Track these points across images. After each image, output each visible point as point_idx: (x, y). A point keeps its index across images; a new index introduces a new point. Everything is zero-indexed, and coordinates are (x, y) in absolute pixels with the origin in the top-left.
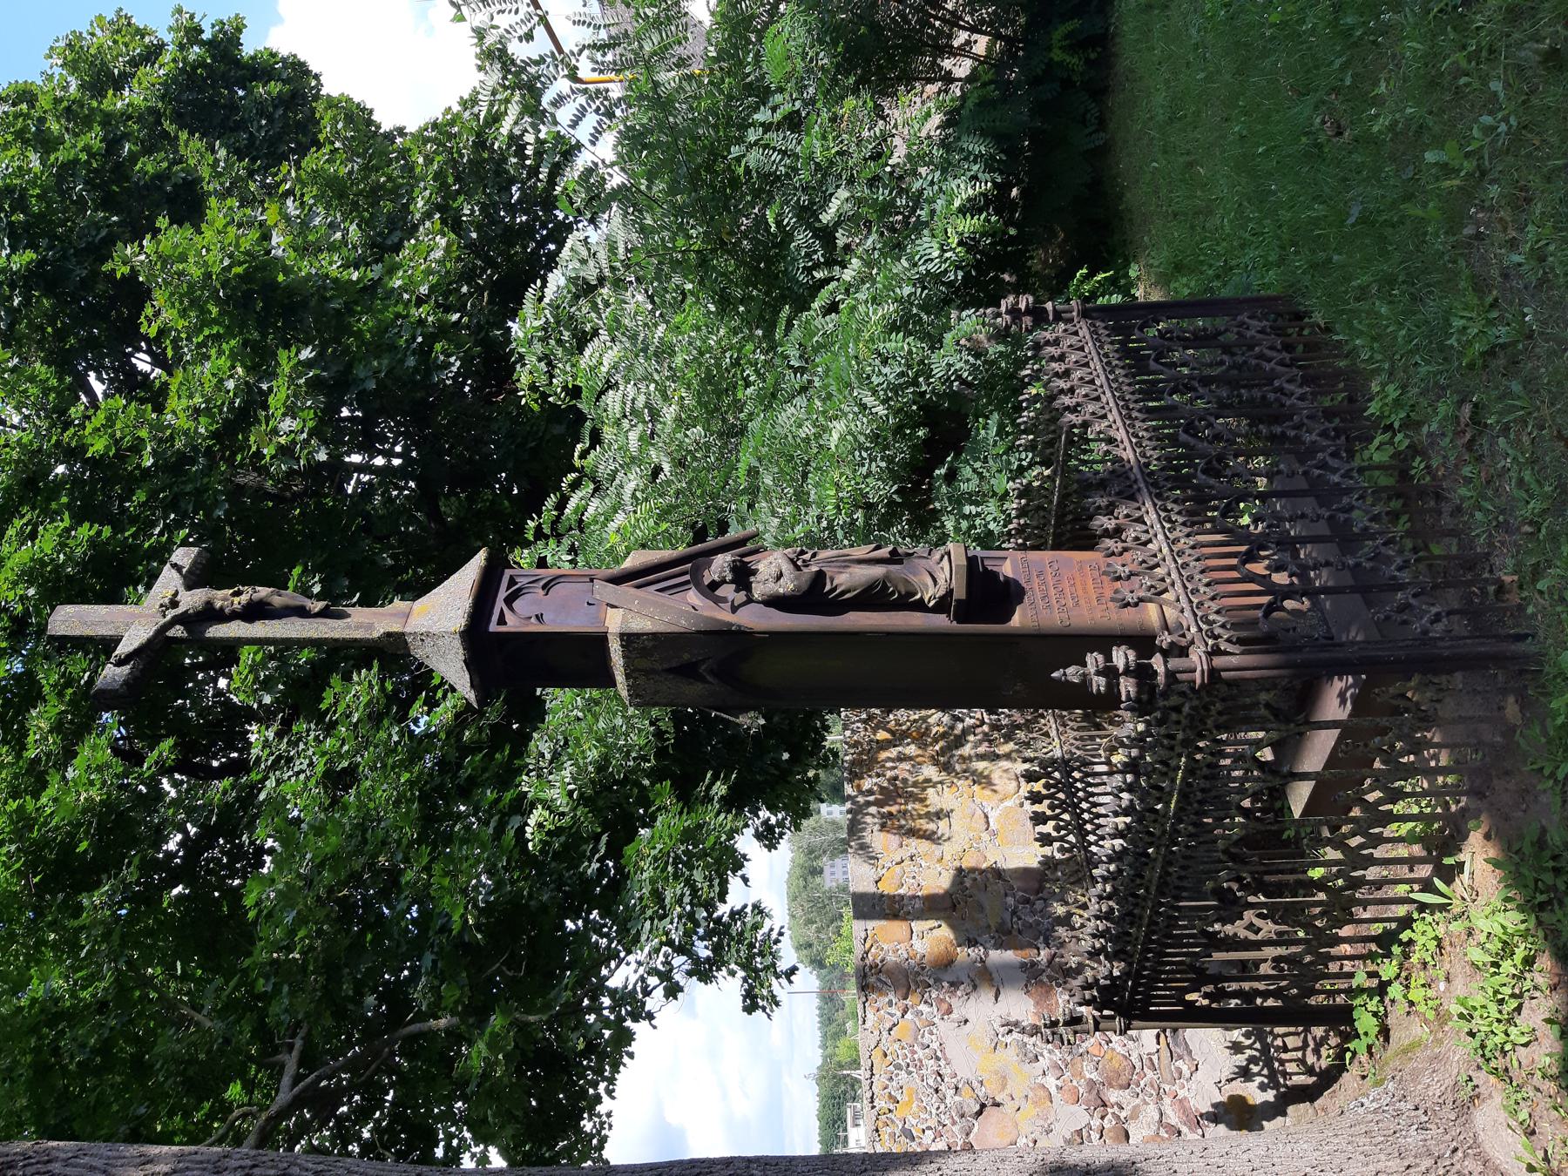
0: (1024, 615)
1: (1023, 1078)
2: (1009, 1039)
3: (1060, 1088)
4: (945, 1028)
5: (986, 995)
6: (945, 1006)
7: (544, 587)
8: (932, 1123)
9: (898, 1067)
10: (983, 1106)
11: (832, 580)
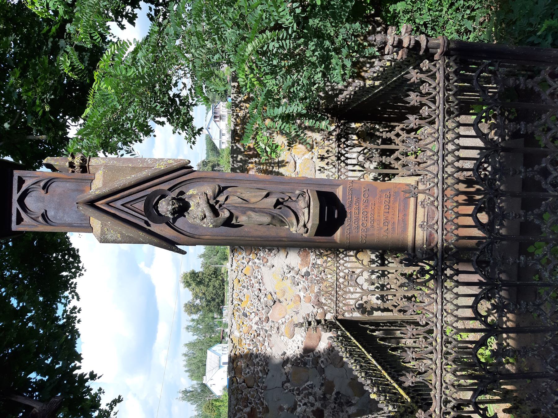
0: (342, 234)
1: (293, 291)
2: (289, 275)
3: (304, 297)
4: (264, 270)
5: (282, 254)
6: (265, 260)
7: (44, 188)
8: (255, 310)
9: (244, 287)
10: (275, 302)
11: (237, 218)
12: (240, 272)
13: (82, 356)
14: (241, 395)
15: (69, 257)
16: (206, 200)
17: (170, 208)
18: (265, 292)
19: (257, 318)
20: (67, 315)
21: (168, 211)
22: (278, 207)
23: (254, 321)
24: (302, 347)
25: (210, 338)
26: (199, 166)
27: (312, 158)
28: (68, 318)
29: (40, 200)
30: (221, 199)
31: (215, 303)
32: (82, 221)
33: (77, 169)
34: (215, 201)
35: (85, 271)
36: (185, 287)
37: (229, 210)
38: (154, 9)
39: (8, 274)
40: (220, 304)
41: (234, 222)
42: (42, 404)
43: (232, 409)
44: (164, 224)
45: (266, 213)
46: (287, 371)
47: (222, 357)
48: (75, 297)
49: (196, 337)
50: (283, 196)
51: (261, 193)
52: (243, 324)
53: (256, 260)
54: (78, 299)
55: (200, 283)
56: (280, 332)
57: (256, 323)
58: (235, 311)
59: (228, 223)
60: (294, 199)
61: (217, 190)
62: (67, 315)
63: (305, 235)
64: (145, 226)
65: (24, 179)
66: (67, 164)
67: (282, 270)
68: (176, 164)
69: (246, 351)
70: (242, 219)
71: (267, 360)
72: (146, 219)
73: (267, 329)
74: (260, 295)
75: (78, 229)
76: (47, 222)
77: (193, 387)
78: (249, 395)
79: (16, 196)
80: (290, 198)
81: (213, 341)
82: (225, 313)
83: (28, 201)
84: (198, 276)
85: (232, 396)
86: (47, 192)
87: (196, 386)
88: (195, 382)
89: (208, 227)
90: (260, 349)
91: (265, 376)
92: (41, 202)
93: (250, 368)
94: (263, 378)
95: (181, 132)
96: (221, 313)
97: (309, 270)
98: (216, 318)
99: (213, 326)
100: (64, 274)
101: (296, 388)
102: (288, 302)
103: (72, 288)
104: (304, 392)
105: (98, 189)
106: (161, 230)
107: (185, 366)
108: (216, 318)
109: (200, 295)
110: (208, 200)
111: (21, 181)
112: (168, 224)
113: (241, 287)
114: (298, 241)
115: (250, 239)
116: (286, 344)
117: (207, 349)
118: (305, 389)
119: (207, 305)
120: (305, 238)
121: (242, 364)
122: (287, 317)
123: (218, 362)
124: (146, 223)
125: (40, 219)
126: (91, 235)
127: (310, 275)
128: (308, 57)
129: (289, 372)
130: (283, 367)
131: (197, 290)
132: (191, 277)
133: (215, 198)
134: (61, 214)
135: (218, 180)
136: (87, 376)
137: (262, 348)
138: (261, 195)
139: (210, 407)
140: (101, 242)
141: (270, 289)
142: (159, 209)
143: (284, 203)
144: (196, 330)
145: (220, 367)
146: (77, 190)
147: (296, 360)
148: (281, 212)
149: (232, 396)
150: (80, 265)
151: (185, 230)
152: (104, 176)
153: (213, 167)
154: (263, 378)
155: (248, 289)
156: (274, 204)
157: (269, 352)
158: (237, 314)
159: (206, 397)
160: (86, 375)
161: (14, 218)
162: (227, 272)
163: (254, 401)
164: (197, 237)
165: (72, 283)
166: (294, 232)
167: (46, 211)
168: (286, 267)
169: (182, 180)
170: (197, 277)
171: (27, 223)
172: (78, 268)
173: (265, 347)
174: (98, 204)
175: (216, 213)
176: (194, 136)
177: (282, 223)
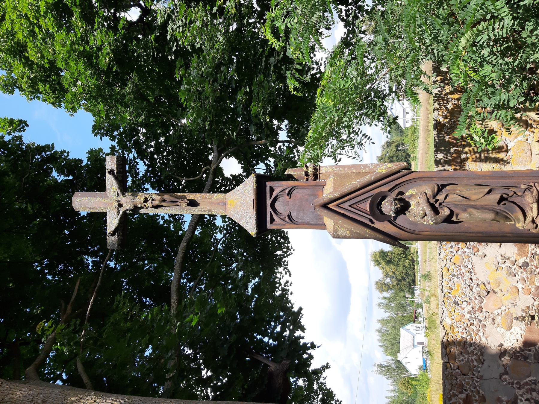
1: (508, 282)
2: (504, 266)
3: (523, 288)
6: (476, 250)
7: (288, 195)
8: (467, 299)
9: (454, 275)
10: (489, 292)
11: (457, 215)
12: (449, 261)
13: (305, 327)
14: (455, 381)
15: (281, 238)
16: (426, 199)
17: (393, 208)
18: (477, 282)
19: (469, 308)
20: (282, 287)
21: (391, 211)
22: (502, 203)
23: (466, 310)
24: (521, 340)
25: (402, 316)
26: (383, 147)
27: (527, 140)
28: (283, 290)
29: (286, 204)
30: (441, 197)
31: (405, 283)
32: (317, 219)
33: (311, 177)
34: (435, 200)
35: (294, 250)
36: (375, 266)
37: (449, 208)
38: (345, 10)
39: (236, 252)
40: (412, 284)
41: (454, 219)
42: (276, 365)
43: (446, 394)
44: (387, 222)
45: (489, 210)
46: (505, 362)
47: (416, 337)
48: (288, 273)
49: (388, 314)
50: (506, 191)
51: (481, 190)
52: (455, 312)
53: (466, 249)
54: (290, 275)
55: (389, 262)
56: (496, 323)
57: (469, 312)
58: (445, 299)
59: (448, 220)
60: (519, 194)
61: (436, 190)
62: (282, 287)
63: (534, 231)
64: (370, 224)
65: (274, 188)
66: (303, 173)
67: (495, 260)
68: (395, 167)
69: (459, 339)
70: (463, 216)
71: (482, 349)
72: (371, 218)
73: (481, 319)
74: (472, 285)
75: (315, 226)
76: (291, 221)
77: (388, 363)
78: (464, 382)
79: (269, 202)
80: (515, 193)
81: (406, 319)
82: (416, 293)
83: (277, 205)
84: (388, 255)
85: (446, 381)
86: (290, 198)
87: (391, 362)
88: (389, 358)
89: (429, 225)
90: (474, 338)
91: (480, 365)
92: (286, 205)
93: (464, 356)
94: (479, 367)
95: (377, 123)
96: (413, 293)
97: (528, 261)
98: (407, 298)
99: (405, 305)
100: (279, 253)
101: (516, 381)
102: (503, 293)
103: (285, 265)
104: (526, 387)
105: (330, 193)
106: (384, 227)
107: (379, 341)
108: (407, 298)
109: (391, 274)
110: (428, 199)
111: (272, 190)
112: (390, 222)
113: (451, 276)
114: (525, 237)
115: (471, 235)
116: (503, 336)
117: (400, 327)
118: (526, 383)
119: (397, 285)
120: (533, 233)
121: (455, 350)
122: (503, 308)
123: (412, 341)
124: (371, 221)
125: (287, 219)
126: (325, 231)
127: (528, 266)
128: (525, 38)
129: (507, 364)
130: (500, 358)
131: (387, 269)
132: (380, 256)
133: (434, 197)
134: (301, 215)
135: (435, 179)
136: (309, 345)
137: (477, 337)
138: (482, 192)
139: (406, 384)
140: (334, 237)
141: (482, 279)
142: (383, 209)
143: (509, 199)
144: (388, 308)
145: (414, 346)
146: (313, 195)
147: (514, 353)
148: (505, 208)
149: (446, 381)
150: (289, 245)
151: (404, 226)
152: (334, 182)
153: (397, 146)
154: (479, 367)
155: (458, 278)
156: (497, 201)
157: (484, 341)
158: (447, 302)
159: (402, 374)
160: (308, 343)
161: (268, 219)
162: (417, 252)
163: (469, 388)
164: (417, 233)
165: (285, 261)
166: (521, 228)
167: (290, 213)
168: (500, 257)
169: (399, 182)
170: (386, 256)
171: (277, 223)
172: (288, 248)
173: (480, 336)
174: (330, 206)
175: (436, 211)
176: (390, 126)
177: (507, 218)
